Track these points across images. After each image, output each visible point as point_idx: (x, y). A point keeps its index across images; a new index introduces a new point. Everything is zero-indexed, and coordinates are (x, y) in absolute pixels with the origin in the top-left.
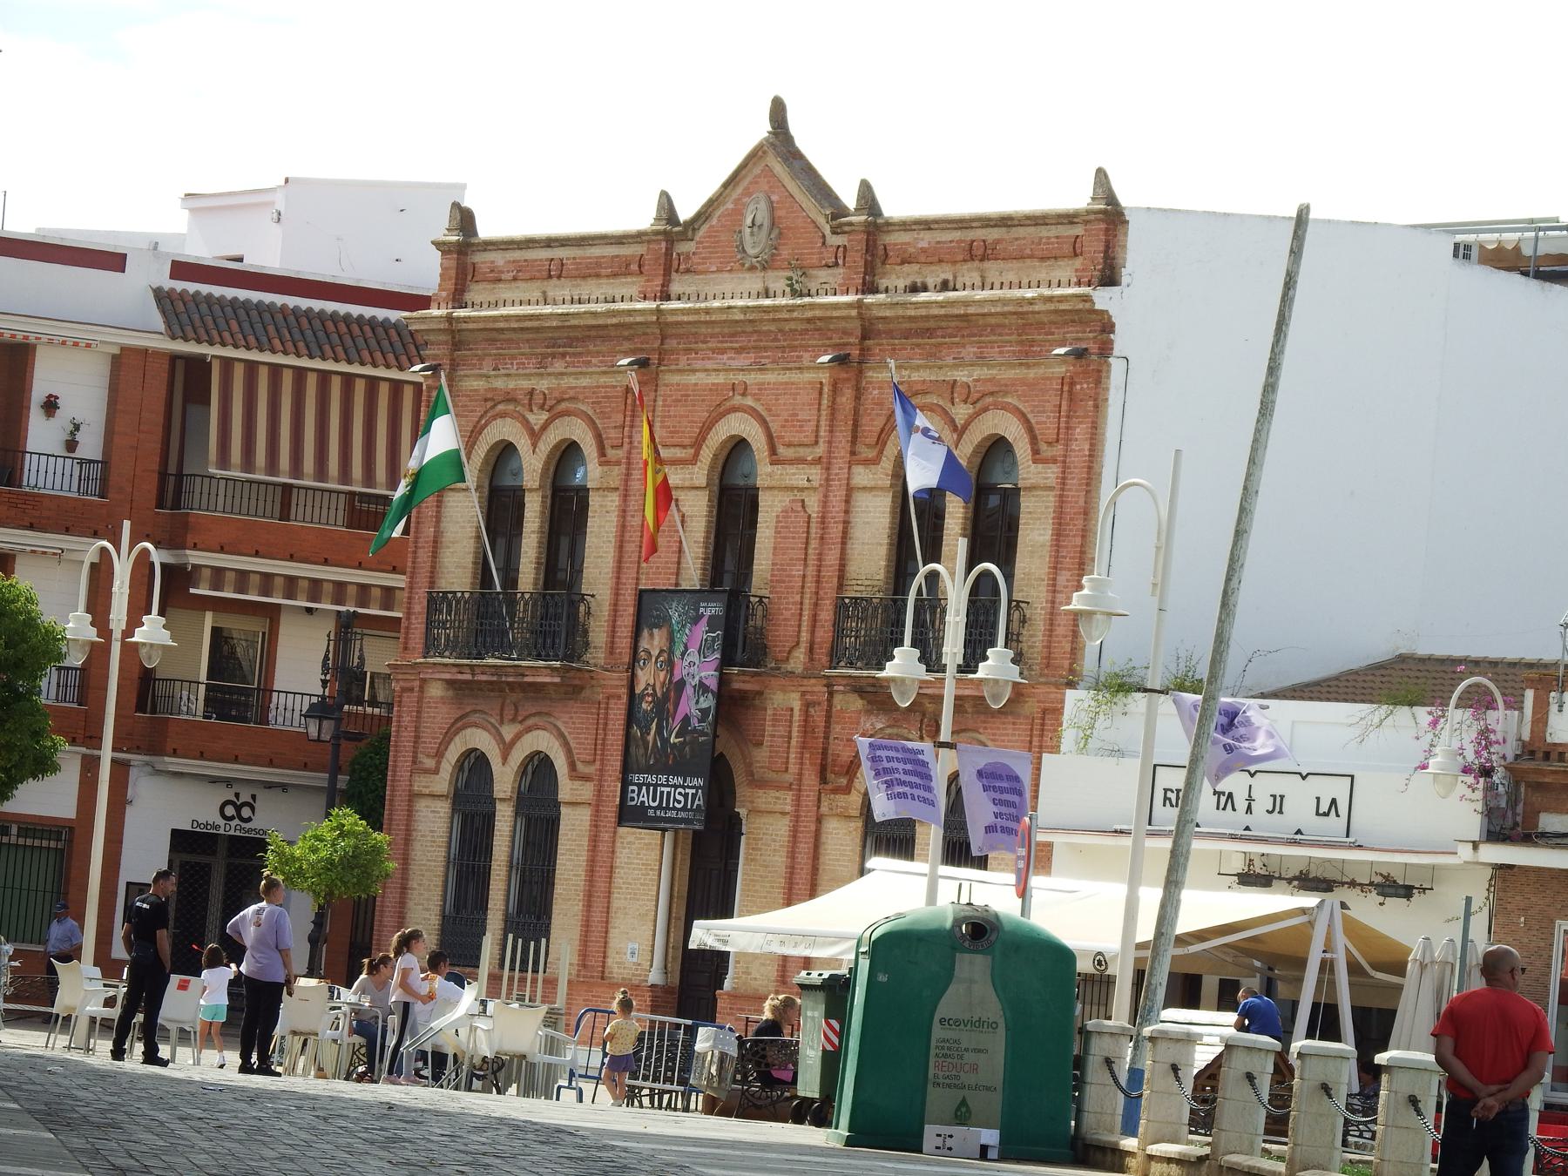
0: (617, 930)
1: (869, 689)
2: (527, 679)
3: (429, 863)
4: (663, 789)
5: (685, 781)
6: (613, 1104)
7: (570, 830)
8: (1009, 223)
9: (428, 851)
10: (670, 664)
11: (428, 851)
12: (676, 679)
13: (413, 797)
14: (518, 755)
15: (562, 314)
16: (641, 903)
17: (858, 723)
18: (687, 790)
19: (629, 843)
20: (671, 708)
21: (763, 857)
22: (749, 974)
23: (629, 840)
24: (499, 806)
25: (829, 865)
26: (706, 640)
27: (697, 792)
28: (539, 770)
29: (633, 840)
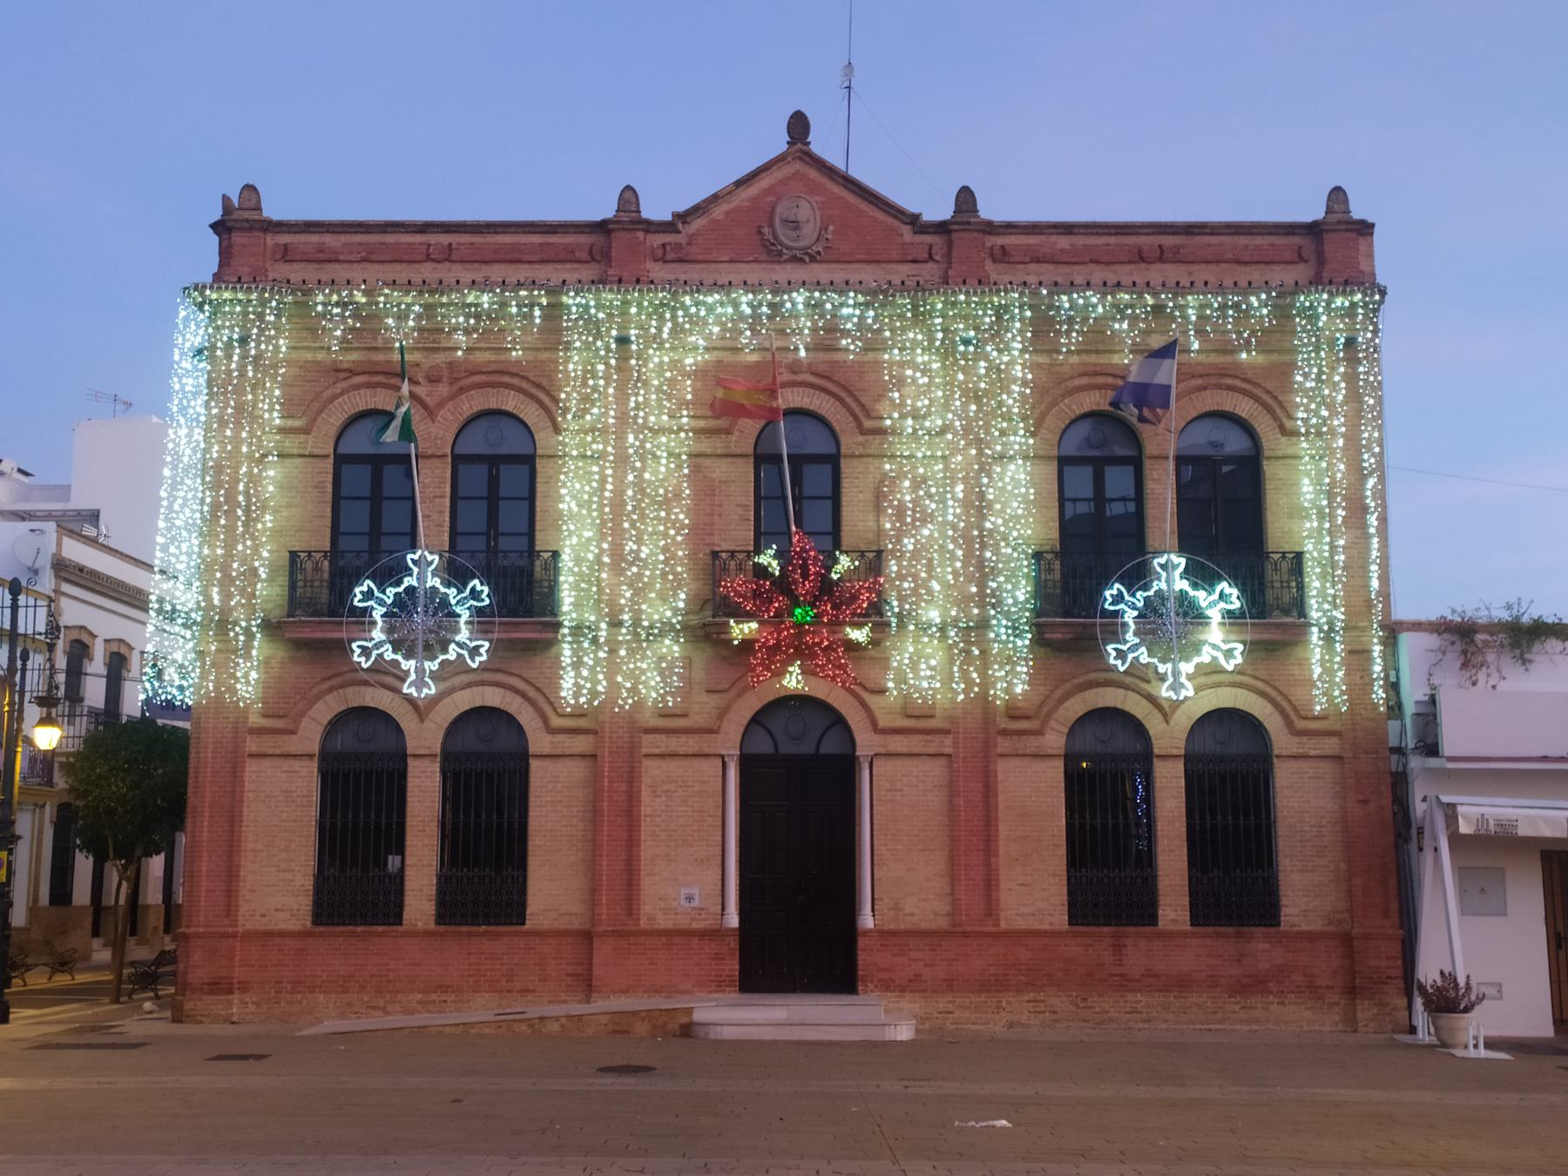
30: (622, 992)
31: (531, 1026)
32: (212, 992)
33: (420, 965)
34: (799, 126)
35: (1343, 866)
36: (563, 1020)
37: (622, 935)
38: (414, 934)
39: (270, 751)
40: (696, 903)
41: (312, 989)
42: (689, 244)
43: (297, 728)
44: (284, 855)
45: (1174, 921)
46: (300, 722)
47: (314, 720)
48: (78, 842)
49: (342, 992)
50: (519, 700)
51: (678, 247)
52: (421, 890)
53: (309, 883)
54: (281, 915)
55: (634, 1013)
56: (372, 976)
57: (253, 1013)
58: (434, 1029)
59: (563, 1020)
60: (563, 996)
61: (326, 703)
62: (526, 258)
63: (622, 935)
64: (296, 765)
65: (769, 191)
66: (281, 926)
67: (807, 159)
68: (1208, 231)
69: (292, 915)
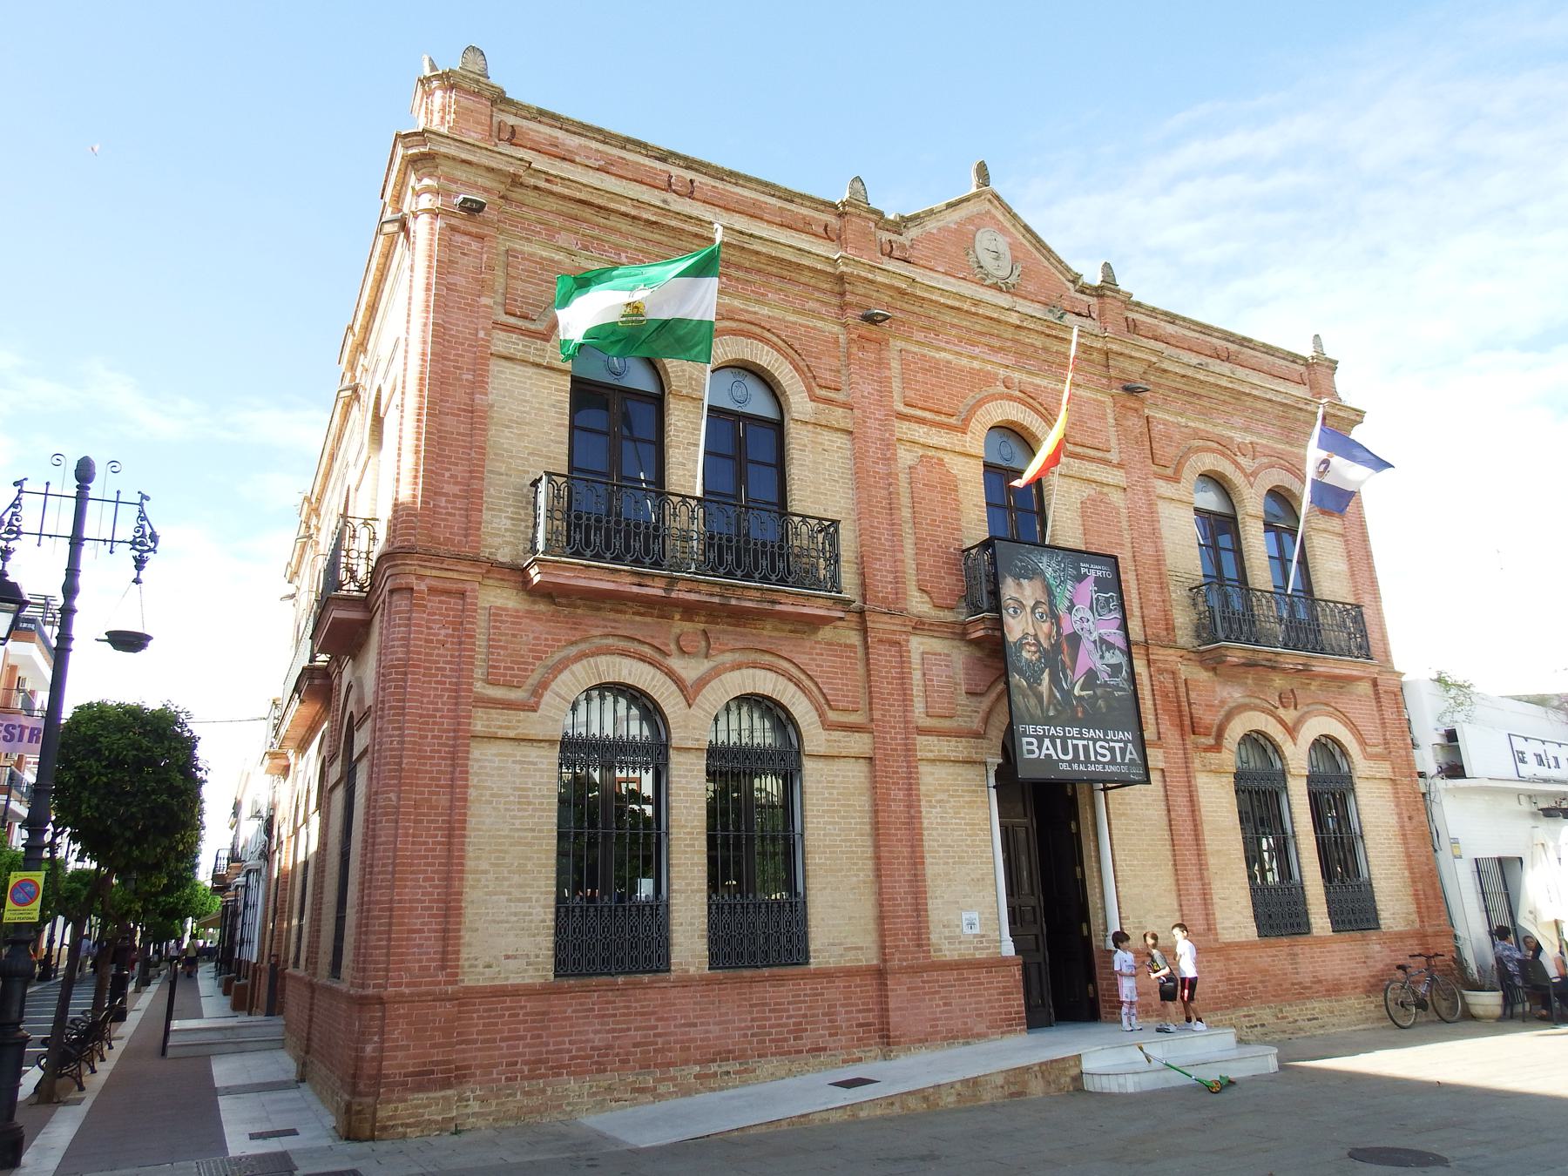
0: (939, 901)
1: (1264, 663)
2: (778, 607)
4: (1075, 742)
5: (1106, 734)
6: (297, 1169)
7: (827, 788)
8: (1246, 344)
9: (514, 817)
10: (1055, 618)
11: (514, 817)
12: (106, 638)
16: (971, 866)
17: (1214, 691)
18: (1112, 744)
19: (939, 801)
20: (1067, 660)
21: (1134, 812)
23: (938, 798)
25: (1207, 816)
26: (1097, 599)
27: (1126, 746)
30: (920, 1041)
31: (926, 1099)
32: (420, 1088)
33: (695, 1025)
34: (982, 172)
35: (1407, 873)
36: (958, 1086)
37: (915, 970)
38: (686, 982)
39: (501, 733)
40: (977, 930)
41: (557, 1070)
42: (911, 247)
43: (538, 704)
44: (516, 879)
45: (1322, 928)
46: (541, 696)
47: (558, 695)
49: (599, 1071)
50: (792, 687)
51: (902, 247)
52: (692, 924)
53: (550, 916)
54: (512, 964)
55: (1027, 1069)
56: (635, 1045)
57: (474, 1114)
58: (817, 1117)
59: (958, 1086)
60: (857, 1053)
61: (573, 673)
62: (766, 216)
63: (915, 970)
64: (533, 753)
65: (970, 220)
66: (515, 980)
67: (996, 202)
68: (1251, 345)
69: (528, 964)
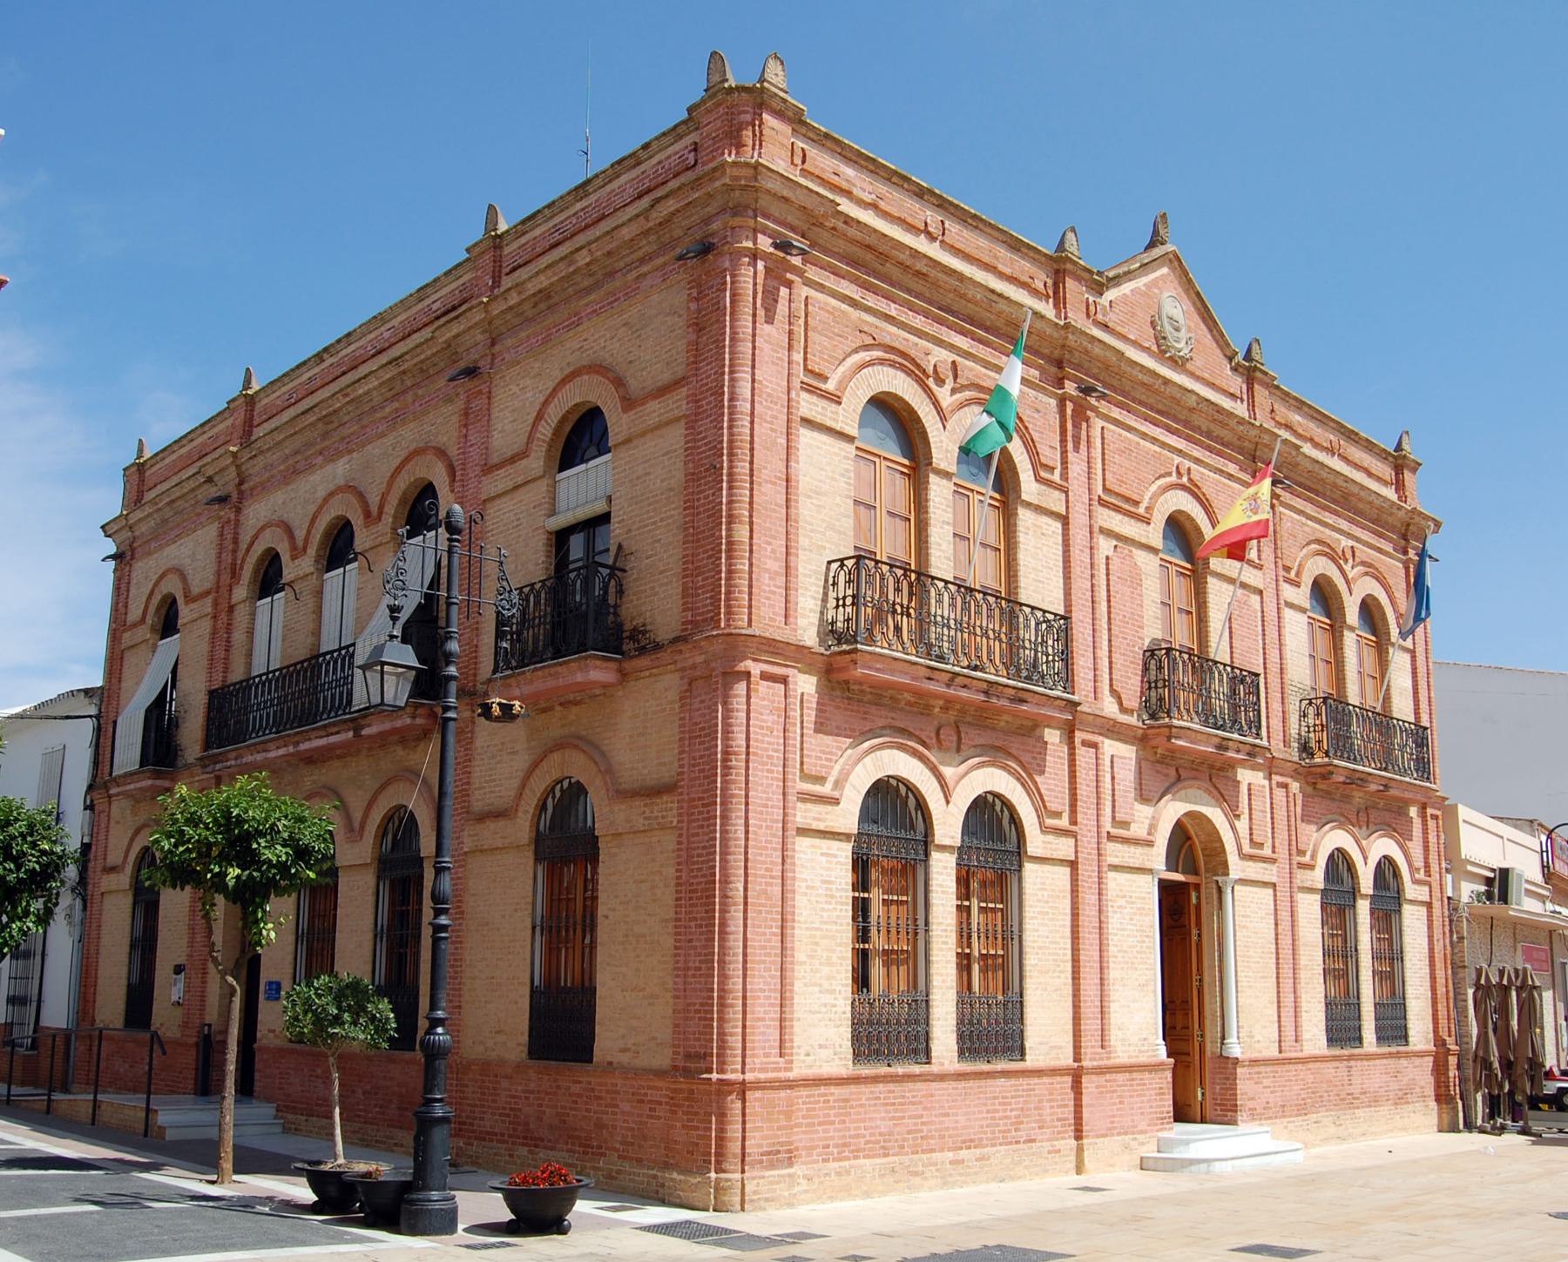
3: (825, 927)
9: (823, 910)
11: (823, 910)
13: (788, 831)
14: (963, 798)
15: (993, 291)
19: (1120, 907)
22: (1253, 1037)
24: (1407, 909)
28: (1386, 872)
29: (1124, 904)
48: (209, 876)
54: (824, 1053)
57: (806, 1191)
